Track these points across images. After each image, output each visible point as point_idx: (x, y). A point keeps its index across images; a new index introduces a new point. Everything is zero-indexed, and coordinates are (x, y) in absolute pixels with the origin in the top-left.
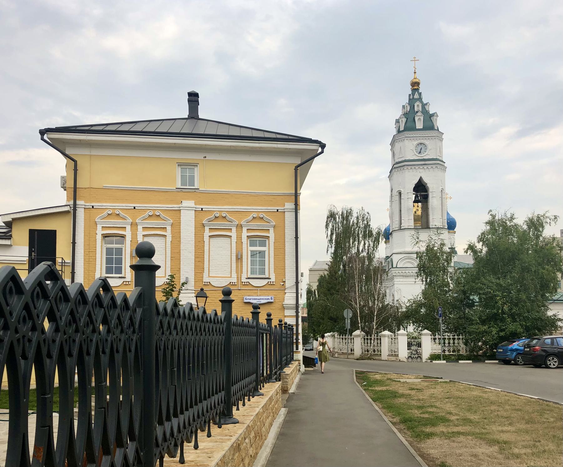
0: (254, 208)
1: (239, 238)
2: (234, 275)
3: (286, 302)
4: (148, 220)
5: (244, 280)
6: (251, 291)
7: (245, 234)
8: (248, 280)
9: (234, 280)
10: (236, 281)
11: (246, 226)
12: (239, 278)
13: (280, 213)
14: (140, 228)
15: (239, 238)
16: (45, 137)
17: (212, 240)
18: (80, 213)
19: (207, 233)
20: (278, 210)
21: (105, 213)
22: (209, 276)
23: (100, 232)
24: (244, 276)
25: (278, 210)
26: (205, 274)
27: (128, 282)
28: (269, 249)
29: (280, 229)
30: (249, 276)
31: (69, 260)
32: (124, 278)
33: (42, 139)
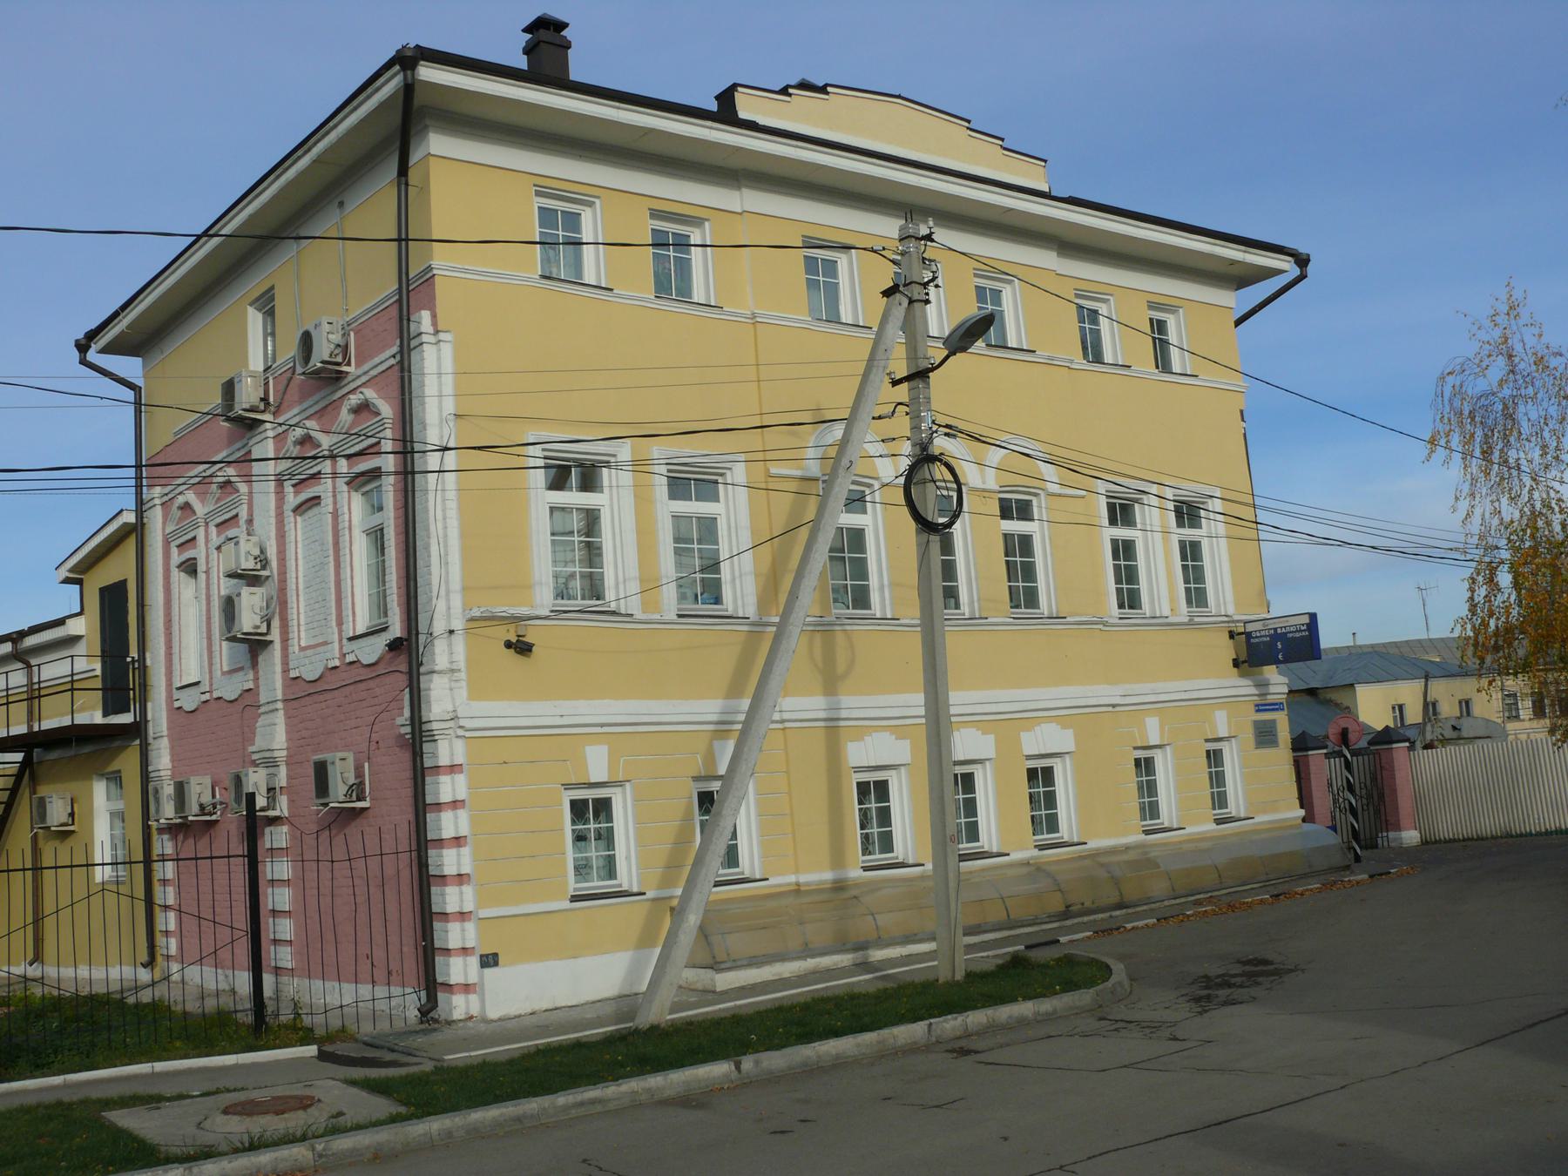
16: (92, 356)
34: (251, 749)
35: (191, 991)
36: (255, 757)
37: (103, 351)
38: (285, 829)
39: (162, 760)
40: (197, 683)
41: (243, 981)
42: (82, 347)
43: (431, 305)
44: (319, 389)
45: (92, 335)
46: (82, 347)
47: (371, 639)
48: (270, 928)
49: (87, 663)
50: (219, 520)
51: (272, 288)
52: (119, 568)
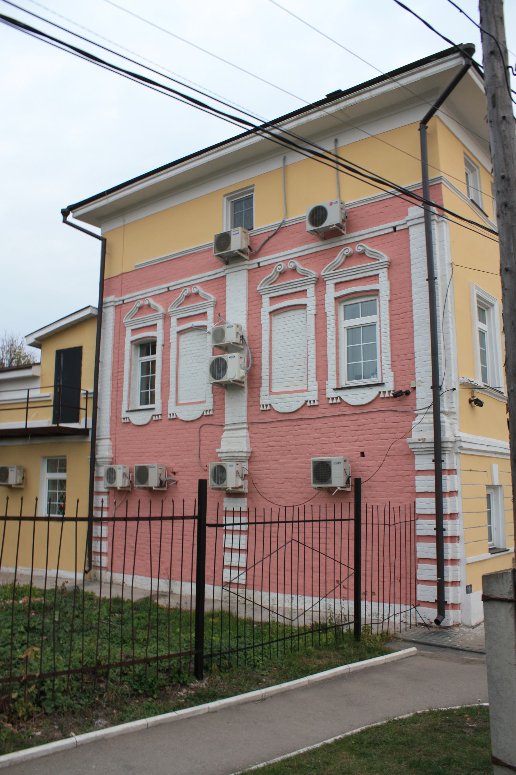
0: (155, 288)
1: (320, 305)
2: (314, 385)
3: (415, 436)
4: (186, 304)
5: (331, 394)
6: (347, 418)
7: (331, 293)
8: (339, 393)
9: (313, 396)
10: (316, 397)
11: (331, 277)
12: (322, 390)
13: (400, 234)
14: (174, 320)
15: (320, 305)
16: (70, 218)
17: (183, 338)
18: (110, 314)
19: (267, 307)
20: (395, 228)
21: (272, 273)
22: (177, 404)
23: (129, 337)
24: (331, 384)
25: (395, 228)
26: (264, 390)
27: (158, 415)
28: (382, 317)
29: (399, 267)
30: (344, 382)
31: (91, 390)
32: (382, 384)
33: (65, 221)
34: (217, 450)
35: (391, 626)
36: (219, 455)
37: (77, 218)
38: (246, 499)
39: (105, 450)
40: (204, 402)
41: (189, 589)
42: (65, 213)
43: (491, 183)
44: (313, 241)
45: (72, 208)
46: (65, 213)
47: (191, 407)
48: (96, 546)
49: (44, 390)
50: (133, 327)
51: (253, 186)
52: (84, 339)
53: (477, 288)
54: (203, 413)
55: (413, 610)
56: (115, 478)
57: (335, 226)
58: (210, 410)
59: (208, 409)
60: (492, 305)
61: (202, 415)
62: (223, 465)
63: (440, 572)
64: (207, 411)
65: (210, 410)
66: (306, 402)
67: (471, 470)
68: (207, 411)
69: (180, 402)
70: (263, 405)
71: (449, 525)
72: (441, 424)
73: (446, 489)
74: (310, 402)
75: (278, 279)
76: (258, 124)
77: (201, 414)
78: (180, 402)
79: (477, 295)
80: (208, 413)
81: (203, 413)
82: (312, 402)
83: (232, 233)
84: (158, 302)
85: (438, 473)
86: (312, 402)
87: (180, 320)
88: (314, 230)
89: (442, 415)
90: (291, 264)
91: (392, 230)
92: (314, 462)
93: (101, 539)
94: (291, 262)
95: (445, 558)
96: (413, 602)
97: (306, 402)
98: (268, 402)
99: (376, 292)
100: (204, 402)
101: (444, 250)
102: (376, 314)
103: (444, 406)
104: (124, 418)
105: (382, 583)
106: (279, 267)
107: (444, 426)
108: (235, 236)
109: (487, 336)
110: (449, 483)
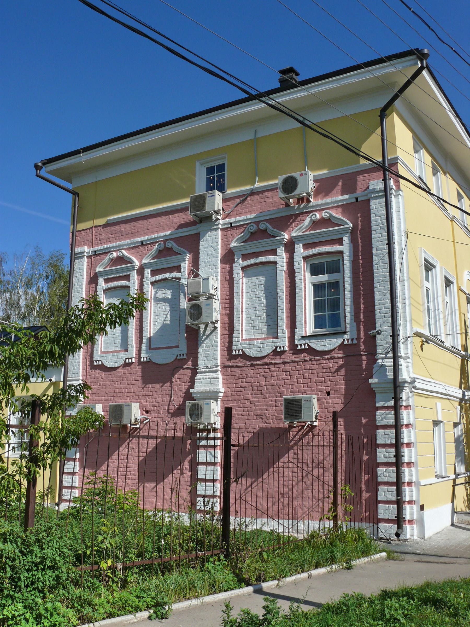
16: (43, 173)
20: (357, 199)
24: (299, 333)
37: (49, 172)
46: (37, 167)
53: (425, 252)
54: (177, 357)
55: (376, 526)
56: (201, 414)
57: (305, 194)
58: (183, 354)
59: (182, 353)
60: (435, 267)
61: (176, 359)
62: (200, 404)
63: (399, 493)
64: (180, 355)
65: (183, 354)
66: (276, 347)
67: (422, 407)
68: (180, 355)
69: (152, 347)
70: (235, 351)
71: (406, 453)
72: (400, 367)
73: (403, 422)
74: (280, 347)
75: (249, 238)
76: (254, 93)
77: (175, 357)
78: (152, 347)
79: (424, 257)
80: (182, 357)
81: (177, 357)
82: (182, 355)
83: (207, 195)
84: (132, 254)
85: (397, 408)
86: (182, 355)
87: (154, 273)
88: (285, 197)
89: (400, 360)
90: (263, 225)
91: (355, 200)
92: (286, 400)
93: (73, 474)
94: (263, 224)
95: (403, 481)
96: (375, 521)
97: (276, 347)
98: (240, 347)
99: (341, 253)
100: (178, 347)
101: (400, 219)
102: (339, 272)
103: (402, 352)
104: (96, 361)
105: (166, 497)
106: (252, 227)
107: (401, 369)
108: (210, 198)
109: (430, 292)
110: (406, 416)
